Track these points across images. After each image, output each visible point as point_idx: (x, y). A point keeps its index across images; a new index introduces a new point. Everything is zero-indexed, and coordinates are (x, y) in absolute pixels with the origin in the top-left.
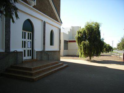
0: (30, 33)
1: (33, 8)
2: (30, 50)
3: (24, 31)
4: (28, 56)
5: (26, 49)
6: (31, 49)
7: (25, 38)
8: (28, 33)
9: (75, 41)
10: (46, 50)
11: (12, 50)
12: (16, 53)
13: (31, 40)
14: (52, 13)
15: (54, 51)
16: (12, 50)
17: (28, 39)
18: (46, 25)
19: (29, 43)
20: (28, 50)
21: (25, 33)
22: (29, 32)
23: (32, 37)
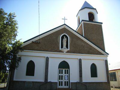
0: (66, 69)
1: (66, 53)
2: (67, 82)
3: (61, 69)
4: (65, 85)
5: (63, 81)
6: (68, 81)
7: (62, 73)
8: (65, 70)
9: (80, 61)
10: (84, 80)
11: (49, 81)
12: (51, 83)
13: (68, 75)
14: (91, 49)
15: (39, 82)
16: (49, 81)
17: (65, 73)
18: (83, 62)
19: (66, 76)
20: (65, 82)
21: (62, 70)
22: (65, 69)
23: (68, 72)
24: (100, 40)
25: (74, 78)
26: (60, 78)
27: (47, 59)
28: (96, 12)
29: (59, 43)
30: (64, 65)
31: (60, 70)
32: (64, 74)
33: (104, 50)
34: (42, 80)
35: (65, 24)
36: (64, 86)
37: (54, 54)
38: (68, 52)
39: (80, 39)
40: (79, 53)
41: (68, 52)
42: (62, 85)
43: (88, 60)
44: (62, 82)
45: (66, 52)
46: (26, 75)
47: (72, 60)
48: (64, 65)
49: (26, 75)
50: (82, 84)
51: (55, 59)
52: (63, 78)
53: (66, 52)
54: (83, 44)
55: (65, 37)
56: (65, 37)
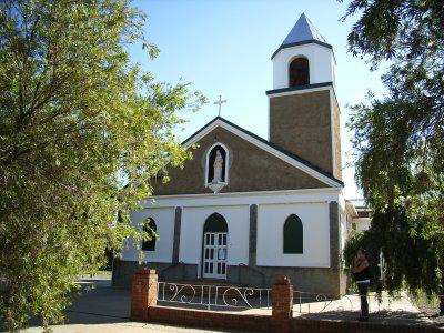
4: (219, 272)
5: (215, 261)
9: (253, 210)
10: (261, 261)
12: (184, 265)
13: (206, 247)
20: (219, 264)
24: (320, 142)
25: (236, 254)
26: (208, 254)
27: (253, 210)
28: (323, 49)
29: (203, 172)
30: (216, 224)
31: (208, 236)
32: (216, 246)
33: (329, 174)
34: (169, 260)
35: (219, 118)
36: (215, 275)
37: (225, 199)
38: (225, 190)
39: (257, 148)
40: (252, 190)
41: (225, 190)
42: (211, 272)
43: (275, 207)
44: (212, 264)
45: (221, 192)
46: (301, 252)
47: (234, 208)
48: (216, 224)
49: (301, 252)
50: (254, 271)
51: (196, 210)
52: (215, 255)
53: (221, 192)
54: (266, 162)
55: (218, 152)
56: (218, 152)
